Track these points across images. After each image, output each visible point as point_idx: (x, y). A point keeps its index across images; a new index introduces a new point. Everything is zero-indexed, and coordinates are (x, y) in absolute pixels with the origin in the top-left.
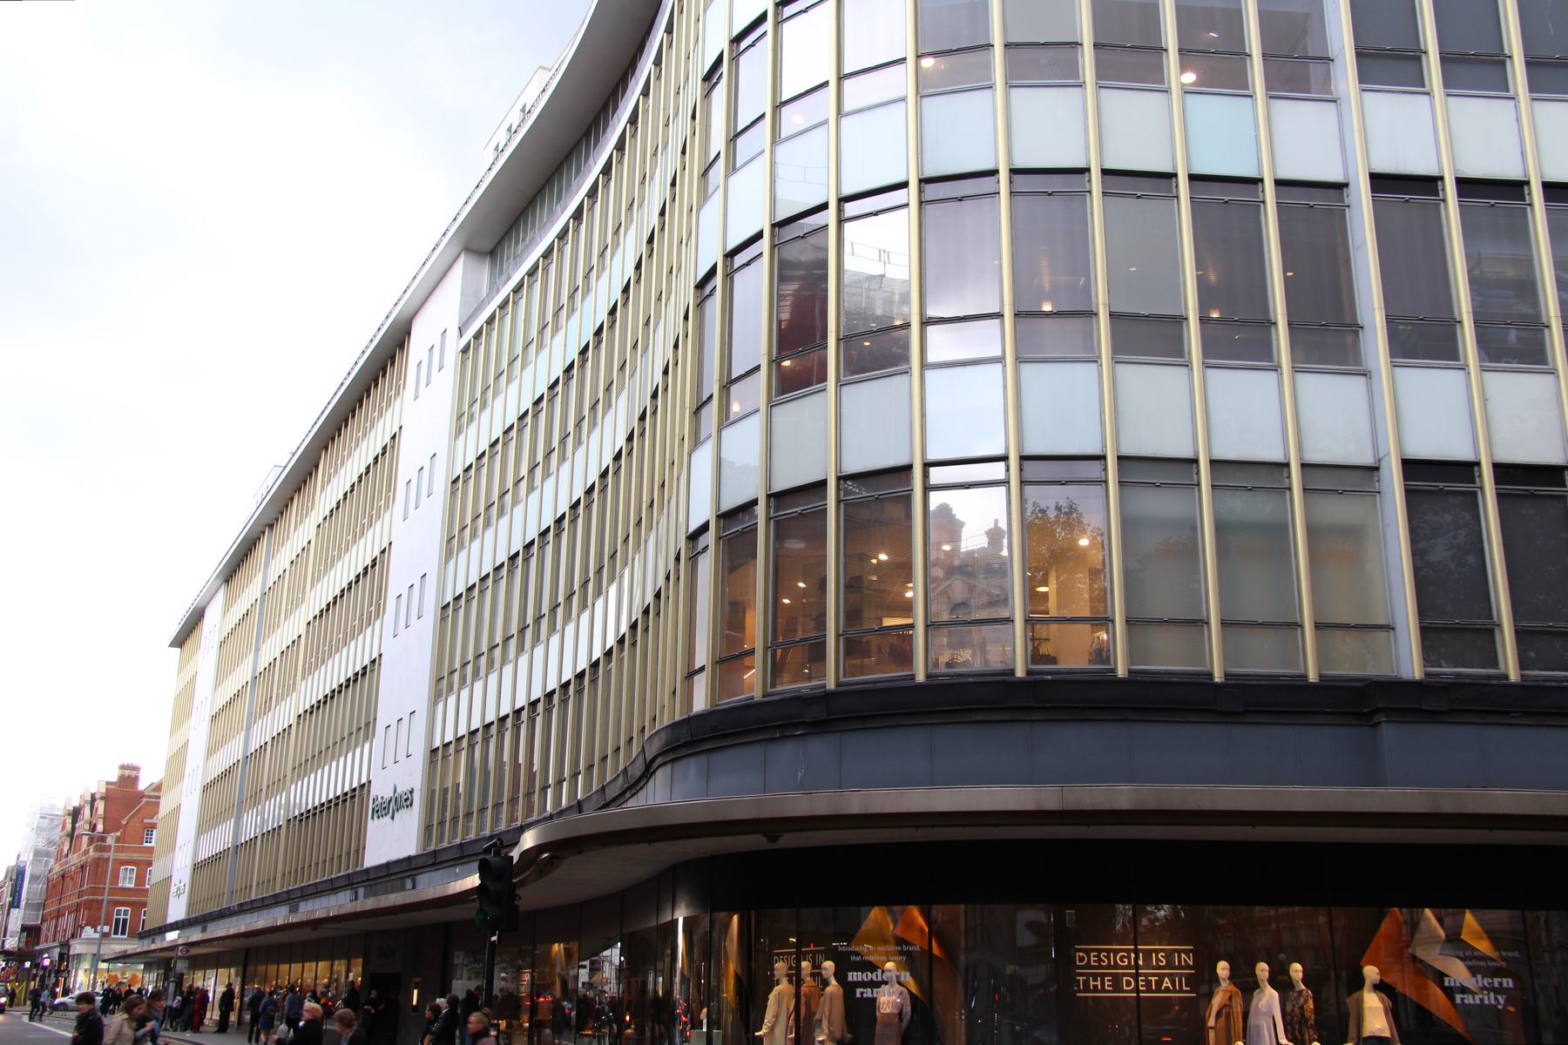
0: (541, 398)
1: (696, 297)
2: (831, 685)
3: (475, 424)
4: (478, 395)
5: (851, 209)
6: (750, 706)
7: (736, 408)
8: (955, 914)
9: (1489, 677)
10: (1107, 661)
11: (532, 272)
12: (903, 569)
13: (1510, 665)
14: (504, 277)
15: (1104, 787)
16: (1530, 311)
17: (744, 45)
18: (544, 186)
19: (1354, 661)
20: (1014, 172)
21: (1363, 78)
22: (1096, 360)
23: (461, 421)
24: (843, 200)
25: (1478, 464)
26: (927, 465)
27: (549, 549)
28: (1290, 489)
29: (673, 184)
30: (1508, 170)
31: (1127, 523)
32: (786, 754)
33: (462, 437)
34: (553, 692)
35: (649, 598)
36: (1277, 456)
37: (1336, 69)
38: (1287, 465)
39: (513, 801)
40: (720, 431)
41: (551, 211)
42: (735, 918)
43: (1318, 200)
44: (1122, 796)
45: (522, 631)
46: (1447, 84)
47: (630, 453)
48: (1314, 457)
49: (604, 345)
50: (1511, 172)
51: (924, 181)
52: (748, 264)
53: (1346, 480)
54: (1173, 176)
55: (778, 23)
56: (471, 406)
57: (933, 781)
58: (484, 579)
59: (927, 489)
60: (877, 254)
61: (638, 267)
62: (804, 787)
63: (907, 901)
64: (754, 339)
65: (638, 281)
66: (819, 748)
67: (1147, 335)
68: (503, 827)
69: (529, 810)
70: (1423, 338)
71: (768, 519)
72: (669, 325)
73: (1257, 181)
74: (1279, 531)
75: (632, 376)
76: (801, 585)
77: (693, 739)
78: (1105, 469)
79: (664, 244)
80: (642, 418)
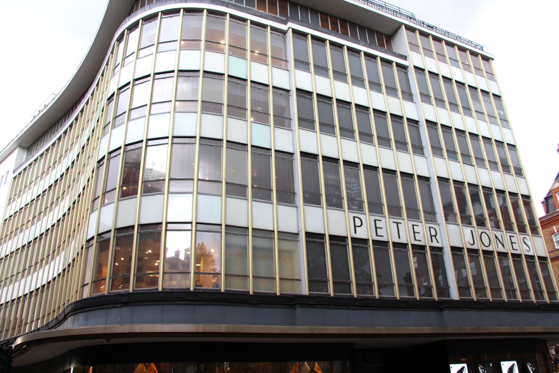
0: (40, 195)
1: (97, 165)
2: (131, 290)
3: (15, 202)
4: (18, 193)
5: (150, 143)
6: (103, 296)
7: (106, 201)
9: (326, 295)
10: (219, 287)
11: (42, 155)
12: (156, 256)
14: (31, 156)
15: (217, 325)
16: (338, 194)
17: (122, 91)
18: (49, 129)
19: (290, 290)
20: (201, 138)
21: (300, 125)
22: (221, 196)
23: (10, 201)
24: (148, 140)
25: (325, 235)
26: (167, 223)
27: (37, 244)
28: (274, 238)
29: (93, 131)
30: (335, 156)
31: (227, 245)
32: (114, 313)
33: (10, 206)
34: (33, 291)
35: (71, 261)
36: (271, 229)
37: (292, 122)
38: (274, 231)
39: (14, 328)
40: (101, 207)
41: (50, 137)
42: (91, 368)
43: (286, 157)
44: (223, 328)
45: (24, 271)
46: (320, 131)
47: (69, 214)
48: (281, 230)
49: (63, 180)
51: (174, 137)
52: (115, 156)
53: (289, 237)
54: (247, 145)
55: (133, 86)
56: (15, 196)
57: (162, 322)
58: (12, 253)
59: (166, 230)
60: (156, 161)
61: (78, 156)
62: (121, 323)
63: (150, 362)
64: (116, 179)
65: (77, 160)
66: (126, 311)
67: (236, 190)
68: (9, 337)
69: (19, 331)
70: (312, 198)
71: (114, 236)
72: (88, 172)
73: (270, 149)
74: (271, 250)
75: (72, 190)
76: (123, 259)
77: (82, 307)
78: (221, 228)
79: (88, 150)
80: (74, 203)
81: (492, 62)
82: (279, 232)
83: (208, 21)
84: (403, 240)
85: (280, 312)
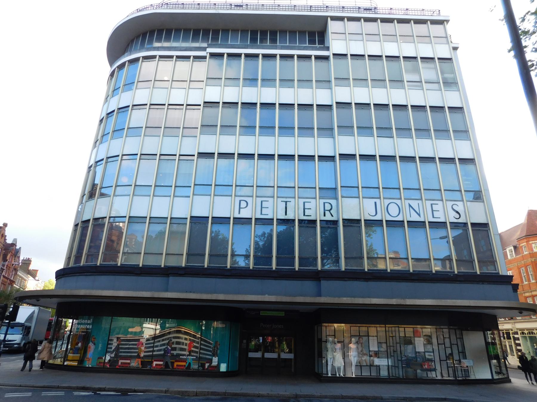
8: (170, 324)
13: (274, 267)
24: (123, 155)
50: (353, 153)
81: (448, 26)
82: (386, 221)
83: (245, 63)
84: (290, 216)
85: (158, 280)
